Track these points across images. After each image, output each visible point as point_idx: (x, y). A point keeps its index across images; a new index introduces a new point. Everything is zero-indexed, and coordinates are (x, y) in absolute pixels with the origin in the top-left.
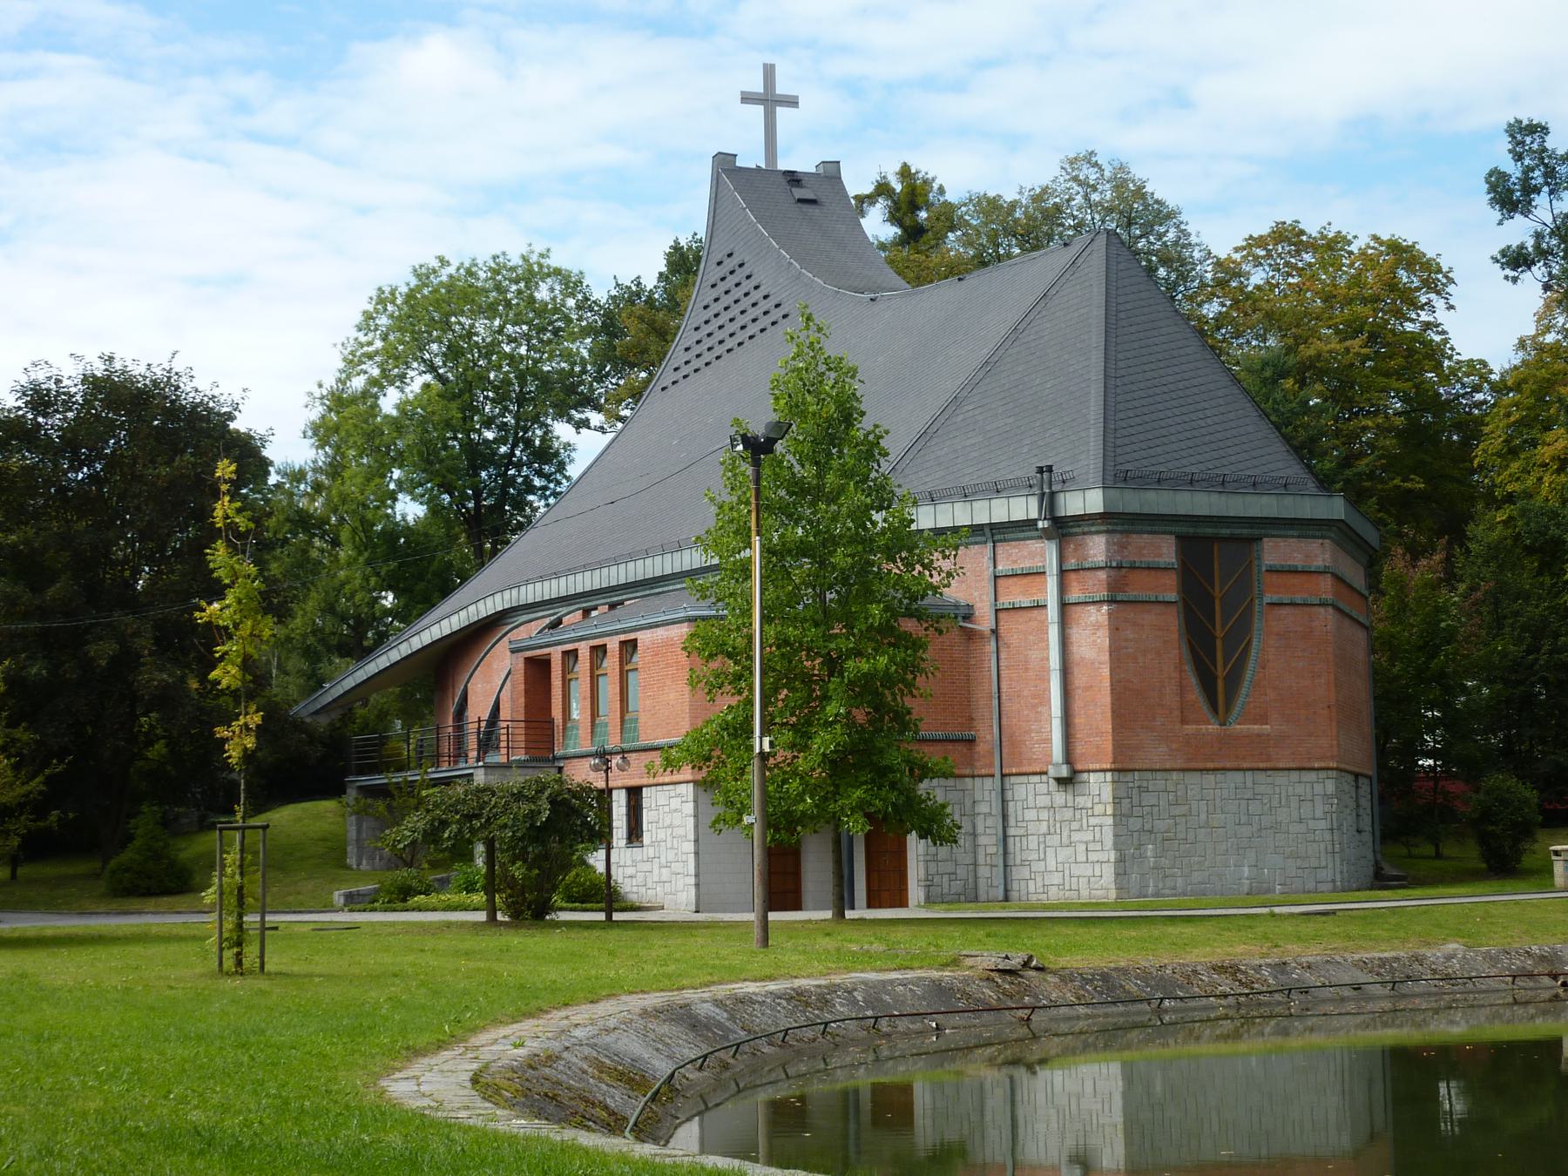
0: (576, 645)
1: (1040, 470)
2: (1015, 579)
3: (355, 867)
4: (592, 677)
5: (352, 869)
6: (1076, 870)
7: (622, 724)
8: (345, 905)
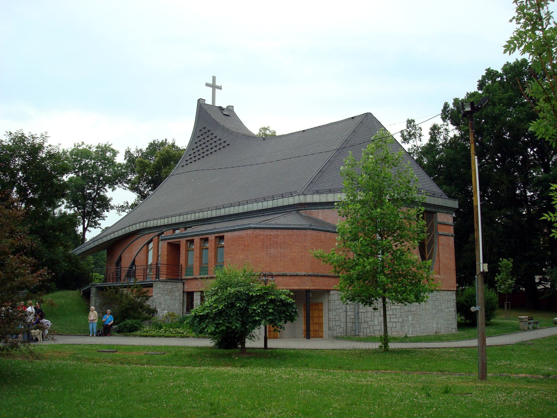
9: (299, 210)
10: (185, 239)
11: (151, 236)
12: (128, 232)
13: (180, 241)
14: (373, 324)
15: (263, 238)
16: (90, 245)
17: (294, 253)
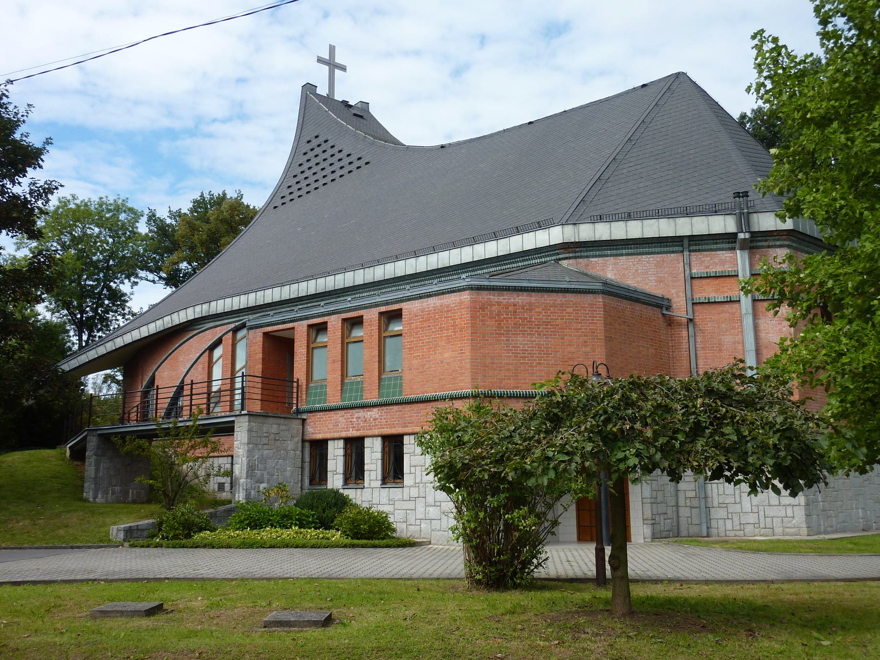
0: (325, 319)
1: (737, 195)
2: (708, 280)
3: (91, 499)
4: (342, 343)
5: (89, 502)
6: (770, 512)
7: (380, 379)
8: (124, 540)
9: (560, 259)
10: (305, 323)
11: (218, 332)
12: (170, 325)
13: (293, 328)
14: (739, 510)
15: (499, 312)
16: (88, 353)
17: (570, 345)
